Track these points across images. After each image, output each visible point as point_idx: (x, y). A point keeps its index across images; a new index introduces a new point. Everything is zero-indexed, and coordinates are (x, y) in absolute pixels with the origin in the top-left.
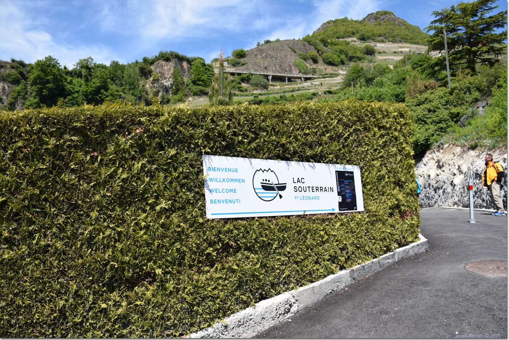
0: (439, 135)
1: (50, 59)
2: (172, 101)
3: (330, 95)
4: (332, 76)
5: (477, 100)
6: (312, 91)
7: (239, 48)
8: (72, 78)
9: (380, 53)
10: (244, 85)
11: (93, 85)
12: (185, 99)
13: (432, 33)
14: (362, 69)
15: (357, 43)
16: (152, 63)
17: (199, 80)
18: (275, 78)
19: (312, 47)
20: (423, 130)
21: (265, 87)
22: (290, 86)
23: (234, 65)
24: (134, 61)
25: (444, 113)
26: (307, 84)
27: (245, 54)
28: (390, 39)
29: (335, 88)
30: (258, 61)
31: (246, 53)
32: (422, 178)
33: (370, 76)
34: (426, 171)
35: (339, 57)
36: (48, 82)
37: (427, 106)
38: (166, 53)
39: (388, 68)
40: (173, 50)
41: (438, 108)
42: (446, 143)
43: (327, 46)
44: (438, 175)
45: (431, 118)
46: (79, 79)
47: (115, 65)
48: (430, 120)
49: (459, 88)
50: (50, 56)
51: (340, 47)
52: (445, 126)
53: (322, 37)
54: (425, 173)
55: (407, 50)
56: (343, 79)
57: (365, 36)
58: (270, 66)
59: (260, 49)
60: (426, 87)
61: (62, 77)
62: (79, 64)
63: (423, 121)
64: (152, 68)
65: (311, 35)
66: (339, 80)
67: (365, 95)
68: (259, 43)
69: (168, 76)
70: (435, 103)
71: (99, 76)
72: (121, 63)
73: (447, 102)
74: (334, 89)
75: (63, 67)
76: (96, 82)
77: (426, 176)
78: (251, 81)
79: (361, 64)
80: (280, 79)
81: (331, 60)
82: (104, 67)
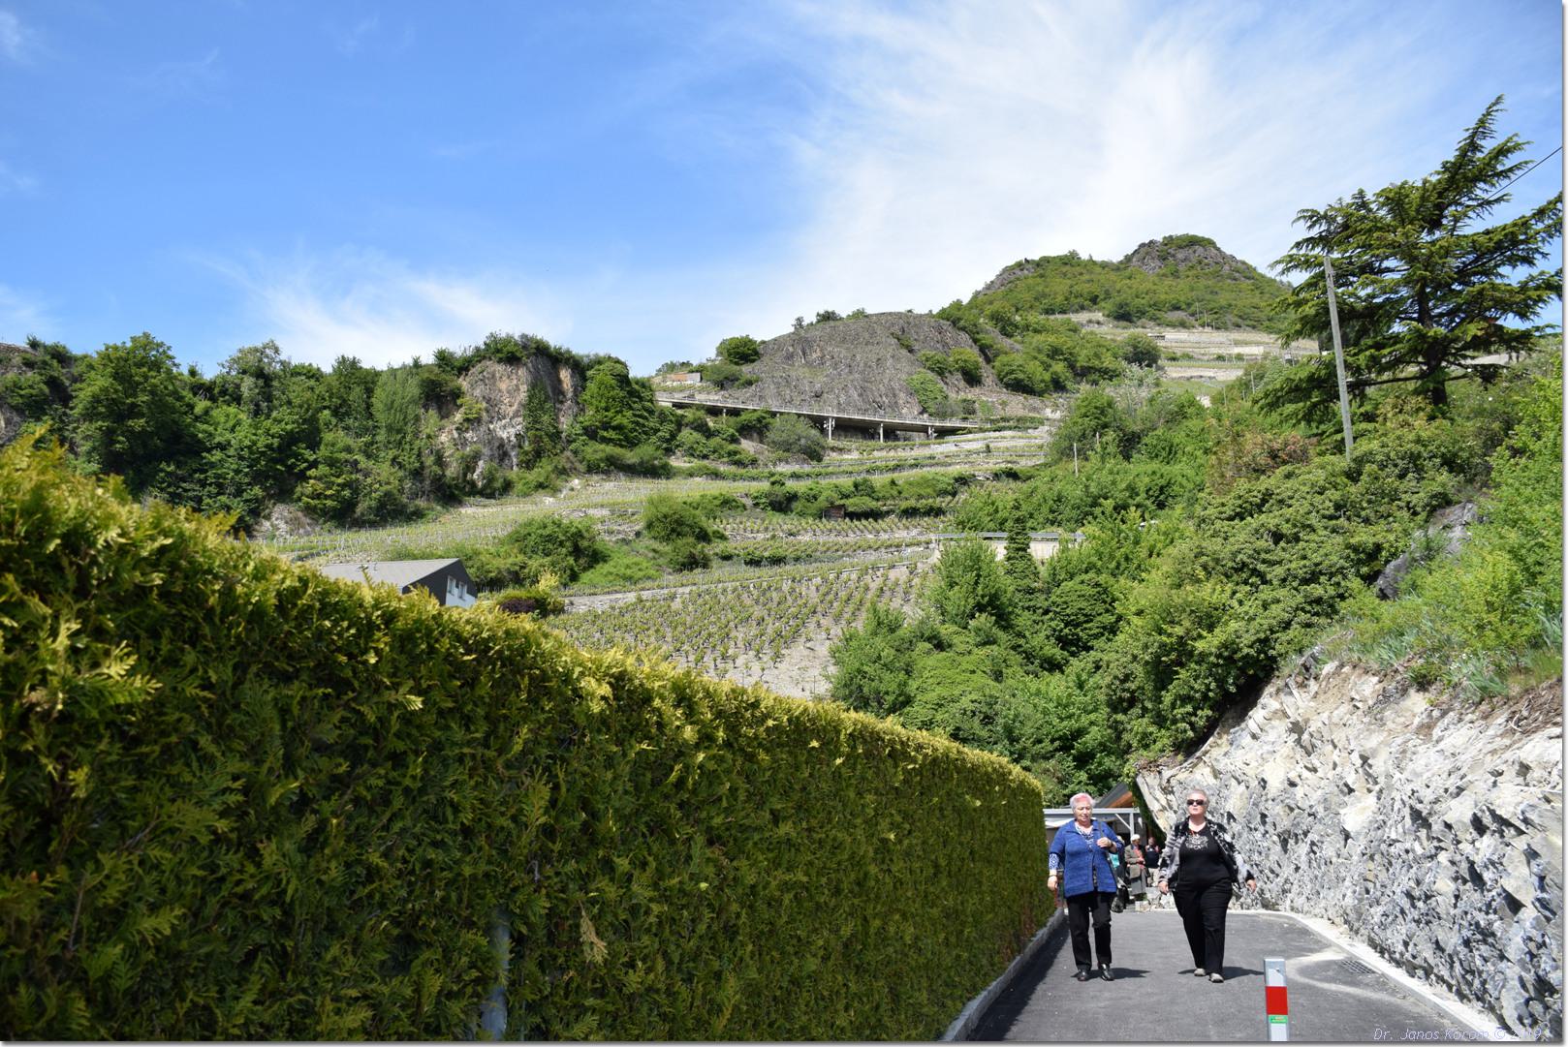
0: (1308, 625)
1: (146, 343)
2: (519, 487)
3: (1013, 484)
4: (1021, 424)
5: (1442, 502)
6: (956, 470)
7: (736, 332)
8: (209, 403)
9: (1174, 359)
10: (748, 446)
11: (275, 429)
12: (559, 483)
13: (1299, 277)
14: (1110, 405)
15: (1104, 329)
16: (464, 367)
17: (606, 426)
18: (845, 427)
19: (964, 336)
20: (1251, 607)
21: (814, 454)
22: (892, 453)
23: (722, 383)
24: (410, 362)
25: (1328, 548)
26: (948, 446)
27: (756, 353)
28: (1207, 318)
29: (1031, 463)
30: (793, 374)
31: (760, 350)
32: (1242, 787)
33: (1136, 428)
34: (1254, 764)
35: (1047, 367)
36: (133, 411)
37: (1270, 519)
38: (509, 340)
39: (1192, 403)
40: (530, 333)
41: (1304, 526)
42: (1331, 656)
43: (1009, 336)
44: (1293, 784)
45: (1280, 563)
46: (232, 410)
47: (349, 369)
48: (1279, 571)
49: (1379, 458)
50: (146, 335)
51: (1051, 339)
52: (1332, 591)
53: (996, 306)
54: (1250, 771)
55: (1257, 351)
56: (1050, 433)
57: (1131, 309)
58: (832, 390)
59: (802, 339)
60: (1273, 455)
61: (180, 398)
62: (234, 361)
63: (1255, 572)
64: (464, 383)
65: (965, 301)
66: (1042, 435)
67: (1114, 483)
68: (799, 320)
69: (511, 411)
70: (1298, 509)
71: (297, 402)
72: (366, 365)
73: (1338, 507)
74: (1023, 465)
75: (186, 372)
76: (284, 420)
77: (1254, 783)
78: (771, 435)
79: (1108, 390)
80: (864, 430)
81: (1021, 376)
82: (313, 374)
